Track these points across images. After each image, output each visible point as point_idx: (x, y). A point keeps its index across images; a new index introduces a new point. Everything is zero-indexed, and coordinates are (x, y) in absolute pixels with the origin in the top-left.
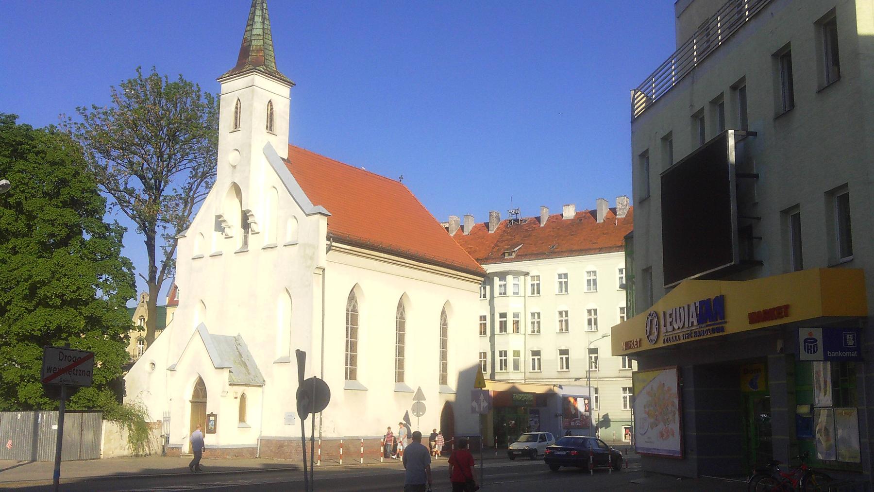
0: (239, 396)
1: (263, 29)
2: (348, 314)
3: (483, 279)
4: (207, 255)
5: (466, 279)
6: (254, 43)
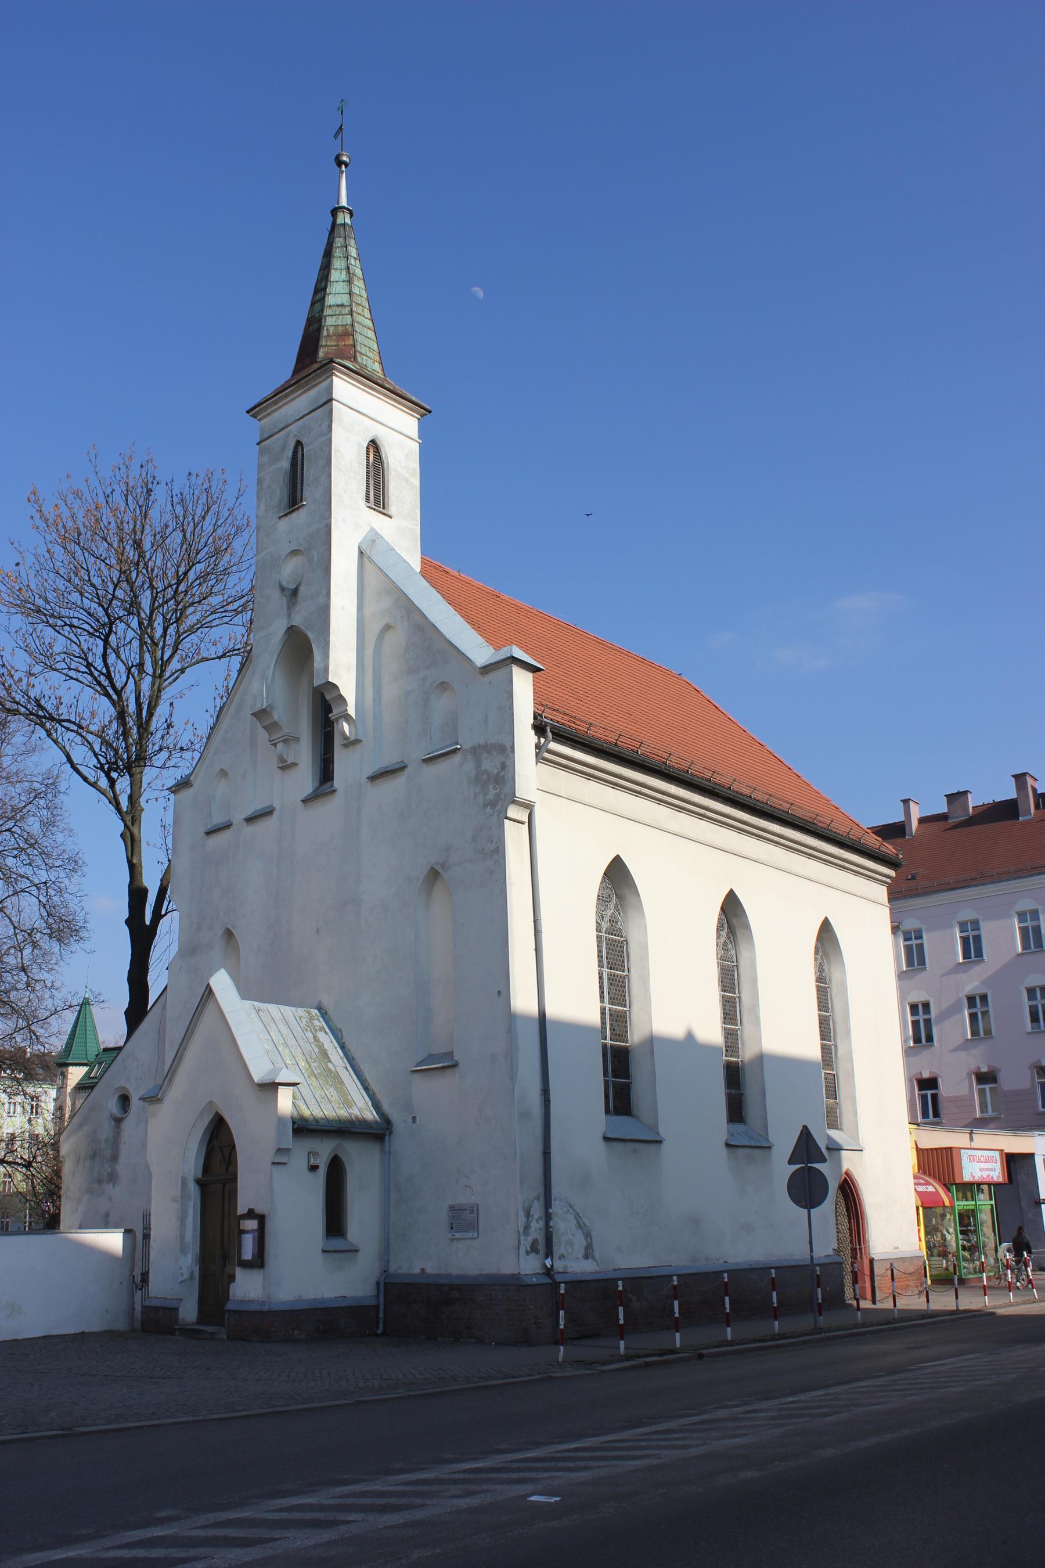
0: (323, 1162)
1: (350, 293)
2: (599, 938)
3: (892, 873)
4: (238, 818)
5: (858, 871)
6: (330, 321)
